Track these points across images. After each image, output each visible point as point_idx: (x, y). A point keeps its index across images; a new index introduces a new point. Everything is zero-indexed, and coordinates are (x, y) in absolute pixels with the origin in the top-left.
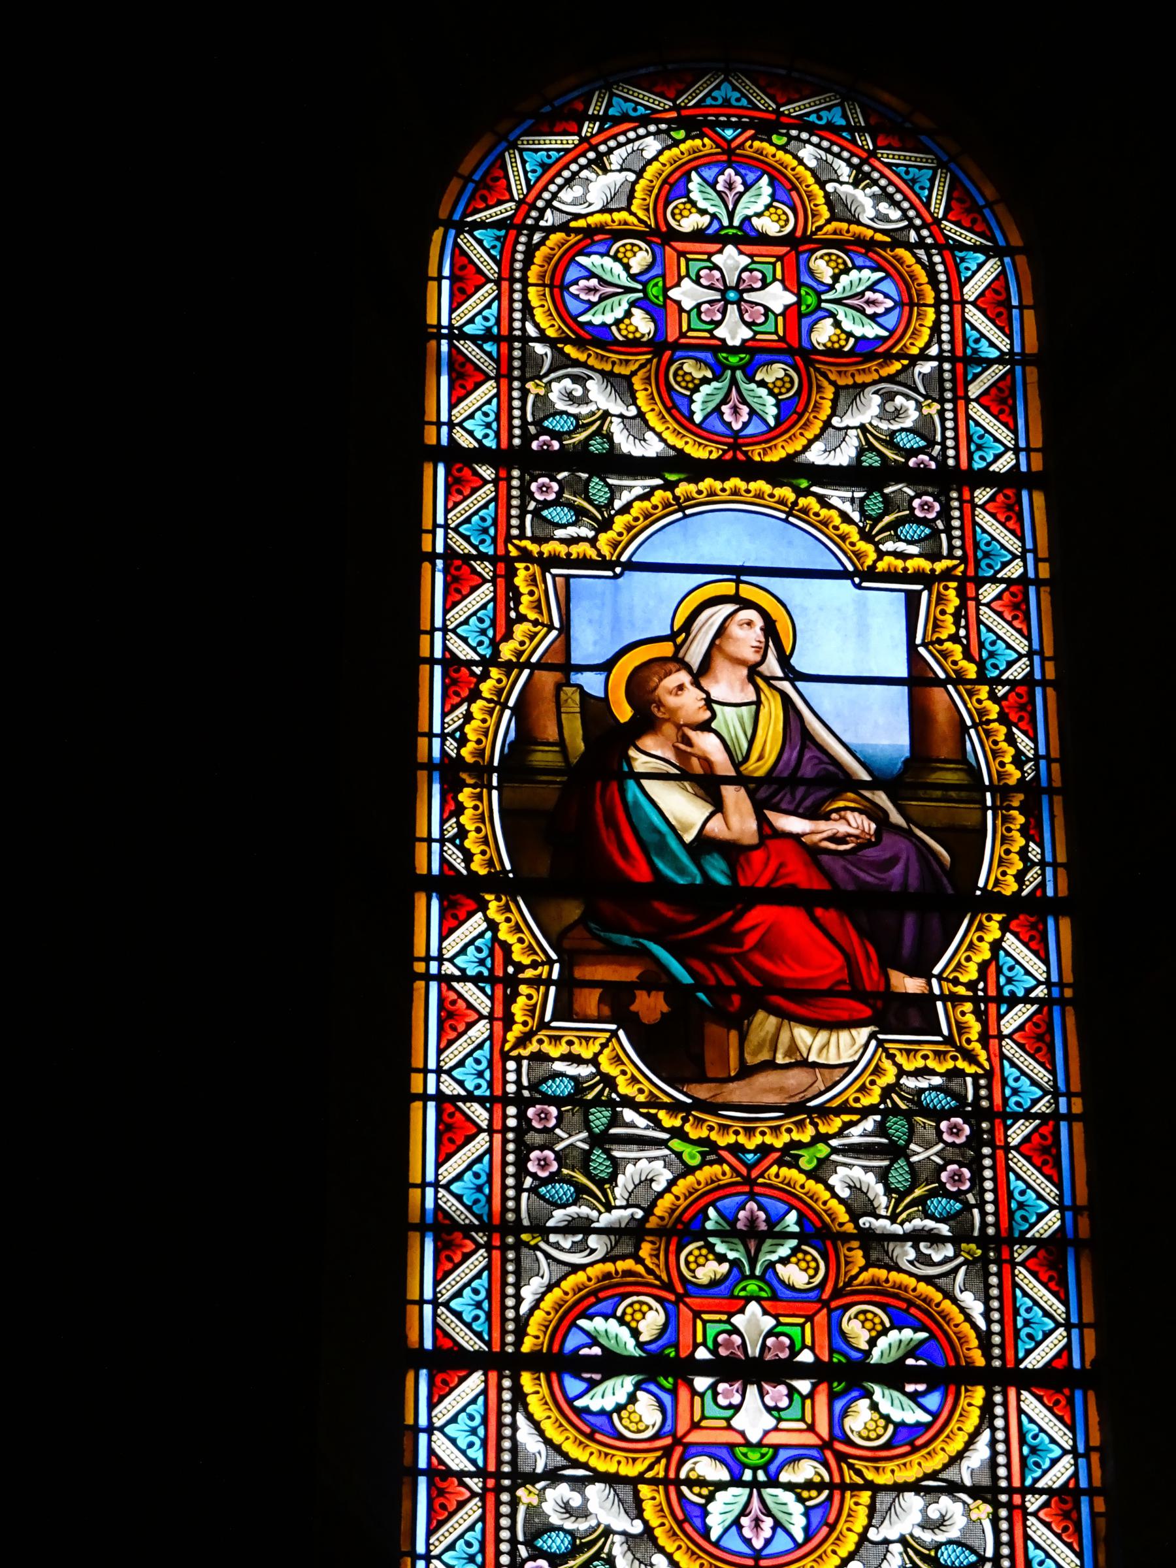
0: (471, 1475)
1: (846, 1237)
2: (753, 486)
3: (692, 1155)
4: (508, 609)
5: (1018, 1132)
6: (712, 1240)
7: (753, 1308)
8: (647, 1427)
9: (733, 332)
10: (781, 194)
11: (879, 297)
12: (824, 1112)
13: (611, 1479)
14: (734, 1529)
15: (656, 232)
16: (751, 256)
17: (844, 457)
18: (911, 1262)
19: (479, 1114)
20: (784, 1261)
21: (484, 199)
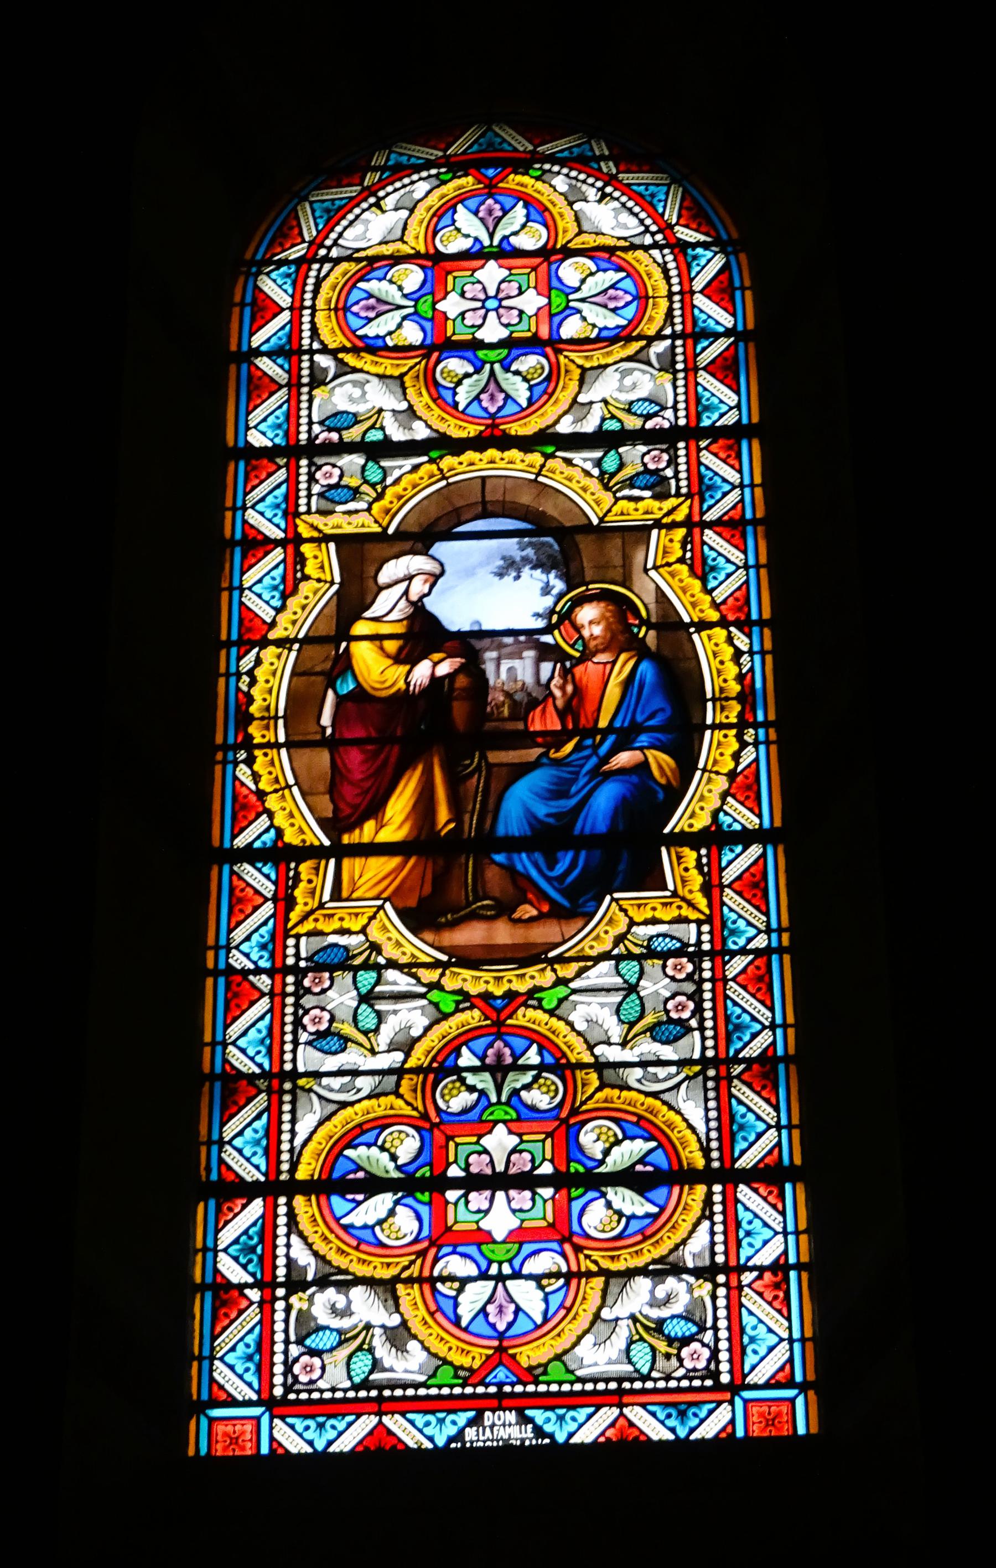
0: (251, 1286)
1: (582, 1066)
2: (507, 454)
3: (448, 1004)
4: (295, 572)
5: (737, 965)
6: (464, 1074)
7: (501, 1128)
8: (405, 1236)
9: (491, 273)
10: (534, 215)
11: (620, 293)
12: (561, 959)
13: (369, 1282)
14: (481, 1316)
15: (426, 256)
16: (510, 269)
17: (589, 426)
18: (639, 1081)
19: (264, 982)
20: (527, 1087)
21: (281, 245)
